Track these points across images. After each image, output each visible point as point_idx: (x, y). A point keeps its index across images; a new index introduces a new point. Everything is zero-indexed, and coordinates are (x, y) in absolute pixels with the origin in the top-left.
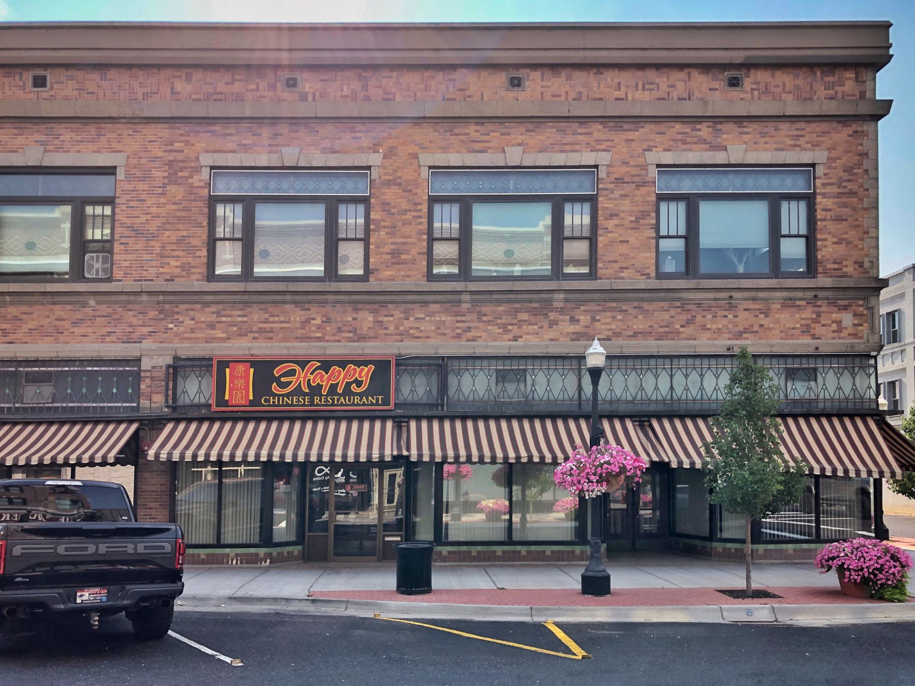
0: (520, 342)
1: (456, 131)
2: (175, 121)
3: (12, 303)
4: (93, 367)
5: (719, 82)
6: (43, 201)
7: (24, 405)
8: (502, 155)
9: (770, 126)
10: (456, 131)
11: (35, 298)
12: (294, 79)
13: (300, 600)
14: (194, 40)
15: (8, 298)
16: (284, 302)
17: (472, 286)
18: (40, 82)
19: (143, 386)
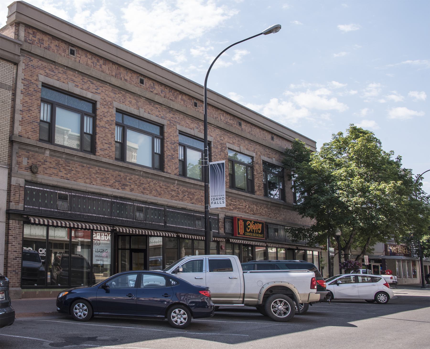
0: (133, 193)
1: (266, 150)
2: (121, 90)
3: (193, 188)
4: (31, 186)
5: (136, 79)
6: (131, 128)
7: (58, 211)
8: (67, 85)
9: (117, 90)
10: (266, 150)
11: (198, 187)
12: (74, 51)
13: (317, 302)
14: (129, 58)
15: (192, 186)
16: (110, 169)
17: (52, 147)
18: (72, 53)
19: (220, 225)
